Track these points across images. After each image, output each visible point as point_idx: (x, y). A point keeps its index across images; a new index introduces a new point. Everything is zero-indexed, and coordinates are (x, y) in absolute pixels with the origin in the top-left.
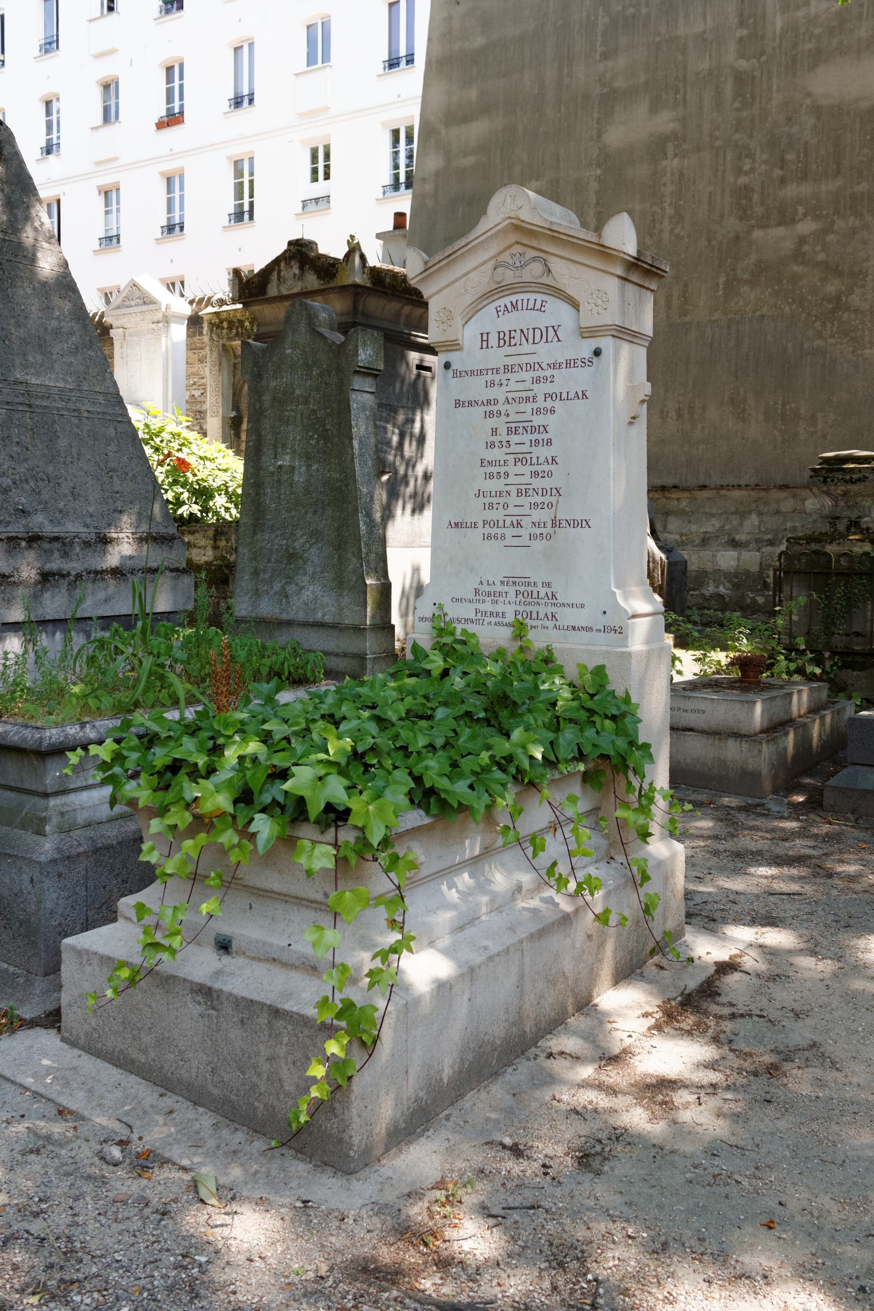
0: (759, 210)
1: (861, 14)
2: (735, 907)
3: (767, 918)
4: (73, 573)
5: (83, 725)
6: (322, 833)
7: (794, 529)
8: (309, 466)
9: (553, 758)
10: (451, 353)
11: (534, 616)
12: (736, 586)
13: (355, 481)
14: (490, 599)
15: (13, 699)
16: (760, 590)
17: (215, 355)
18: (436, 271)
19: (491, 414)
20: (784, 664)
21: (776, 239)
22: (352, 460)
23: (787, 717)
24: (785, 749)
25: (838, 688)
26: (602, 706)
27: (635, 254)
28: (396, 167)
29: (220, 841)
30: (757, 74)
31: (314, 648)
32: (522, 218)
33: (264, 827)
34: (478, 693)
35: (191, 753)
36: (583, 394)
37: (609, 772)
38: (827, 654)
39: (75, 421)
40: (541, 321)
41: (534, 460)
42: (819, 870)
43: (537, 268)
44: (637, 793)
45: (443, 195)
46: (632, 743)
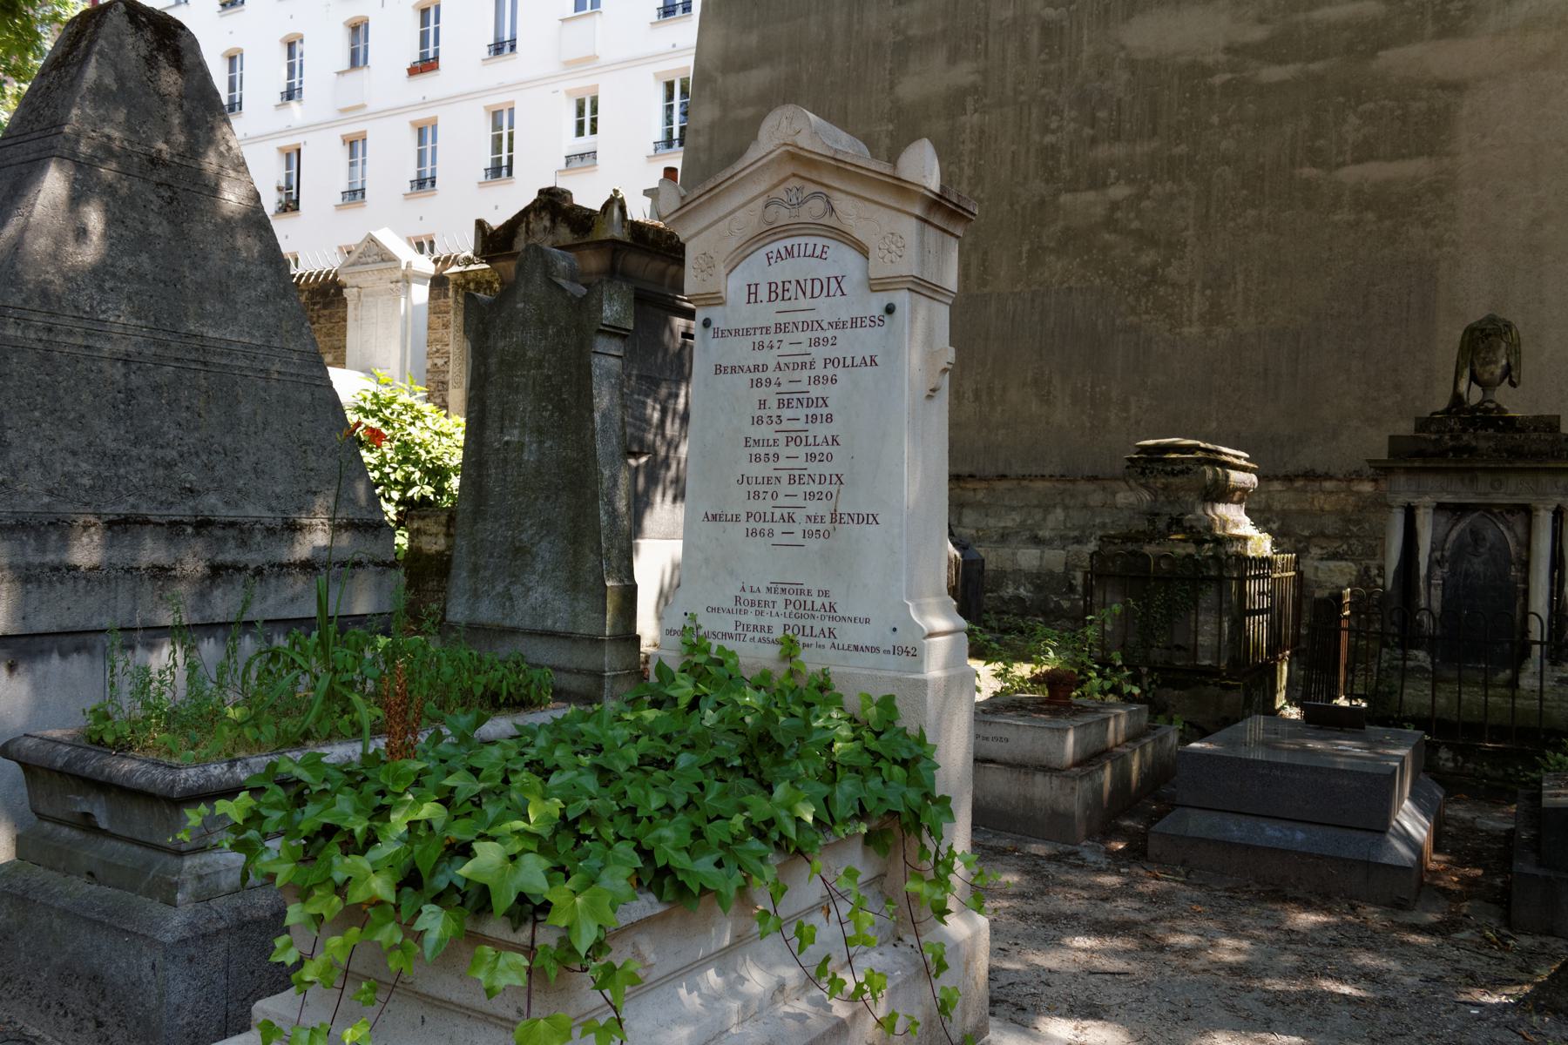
0: (1067, 172)
2: (1050, 992)
3: (1088, 1006)
4: (252, 566)
5: (232, 763)
6: (515, 930)
7: (1104, 525)
8: (541, 443)
9: (827, 820)
10: (712, 309)
11: (808, 631)
12: (1038, 588)
13: (596, 462)
15: (147, 729)
17: (460, 319)
19: (759, 383)
20: (1096, 682)
21: (1085, 204)
22: (593, 436)
23: (1102, 747)
24: (1101, 785)
25: (1158, 709)
26: (893, 747)
27: (937, 190)
28: (669, 121)
29: (377, 939)
30: (1066, 23)
31: (542, 662)
33: (434, 923)
34: (735, 731)
35: (346, 817)
36: (872, 360)
37: (896, 830)
38: (1145, 670)
39: (262, 383)
40: (823, 270)
41: (811, 440)
42: (1147, 941)
43: (818, 206)
44: (932, 860)
45: (711, 127)
46: (927, 796)
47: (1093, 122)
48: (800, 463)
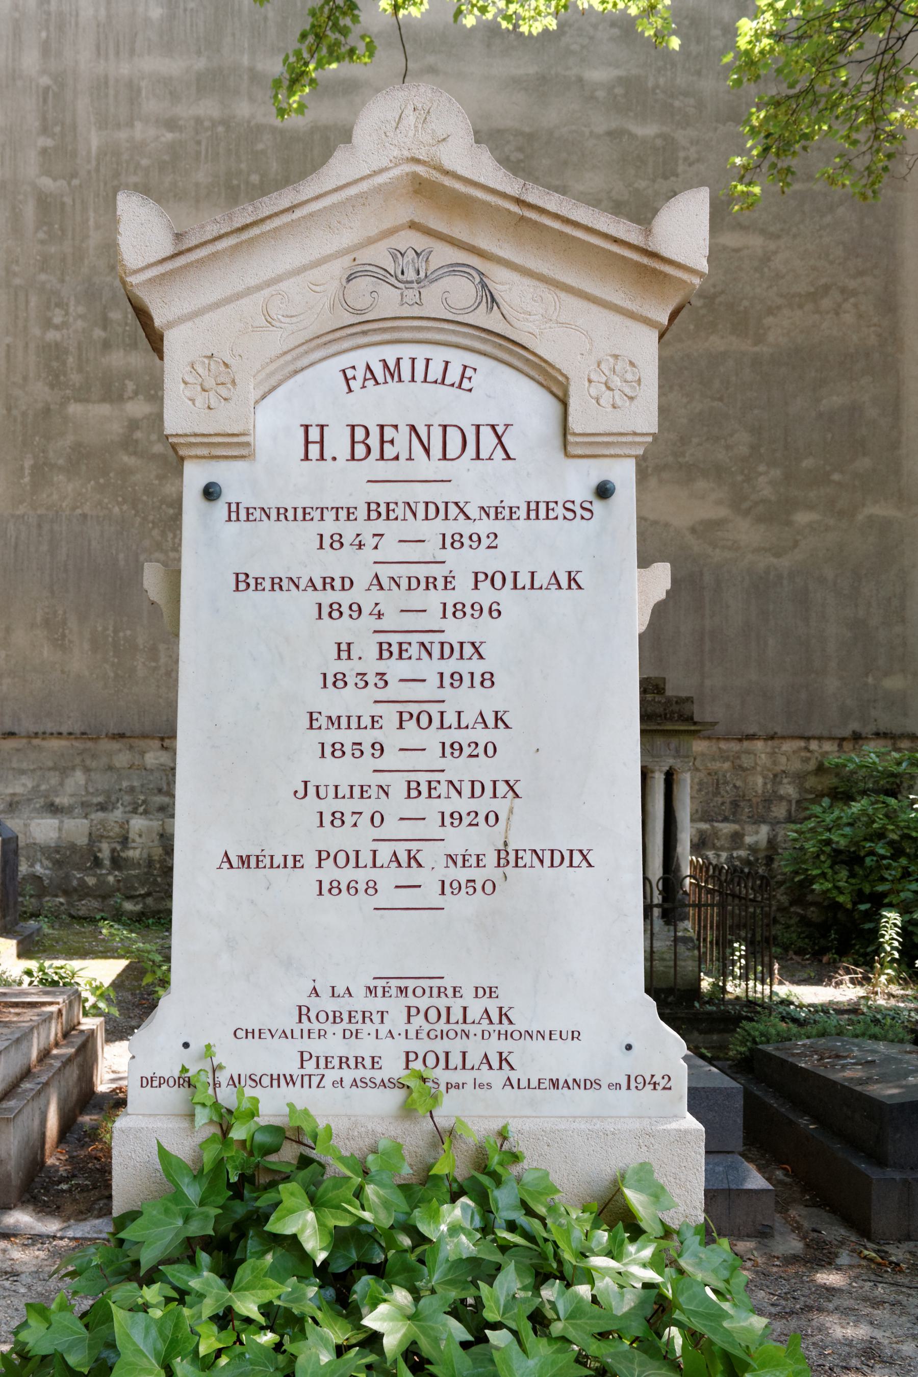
0: (76, 378)
1: (198, 153)
7: (132, 790)
10: (223, 465)
11: (456, 1060)
14: (338, 1028)
16: (90, 868)
18: (201, 262)
19: (335, 611)
30: (68, 200)
32: (448, 165)
40: (464, 410)
47: (105, 323)
48: (431, 758)
